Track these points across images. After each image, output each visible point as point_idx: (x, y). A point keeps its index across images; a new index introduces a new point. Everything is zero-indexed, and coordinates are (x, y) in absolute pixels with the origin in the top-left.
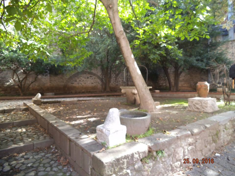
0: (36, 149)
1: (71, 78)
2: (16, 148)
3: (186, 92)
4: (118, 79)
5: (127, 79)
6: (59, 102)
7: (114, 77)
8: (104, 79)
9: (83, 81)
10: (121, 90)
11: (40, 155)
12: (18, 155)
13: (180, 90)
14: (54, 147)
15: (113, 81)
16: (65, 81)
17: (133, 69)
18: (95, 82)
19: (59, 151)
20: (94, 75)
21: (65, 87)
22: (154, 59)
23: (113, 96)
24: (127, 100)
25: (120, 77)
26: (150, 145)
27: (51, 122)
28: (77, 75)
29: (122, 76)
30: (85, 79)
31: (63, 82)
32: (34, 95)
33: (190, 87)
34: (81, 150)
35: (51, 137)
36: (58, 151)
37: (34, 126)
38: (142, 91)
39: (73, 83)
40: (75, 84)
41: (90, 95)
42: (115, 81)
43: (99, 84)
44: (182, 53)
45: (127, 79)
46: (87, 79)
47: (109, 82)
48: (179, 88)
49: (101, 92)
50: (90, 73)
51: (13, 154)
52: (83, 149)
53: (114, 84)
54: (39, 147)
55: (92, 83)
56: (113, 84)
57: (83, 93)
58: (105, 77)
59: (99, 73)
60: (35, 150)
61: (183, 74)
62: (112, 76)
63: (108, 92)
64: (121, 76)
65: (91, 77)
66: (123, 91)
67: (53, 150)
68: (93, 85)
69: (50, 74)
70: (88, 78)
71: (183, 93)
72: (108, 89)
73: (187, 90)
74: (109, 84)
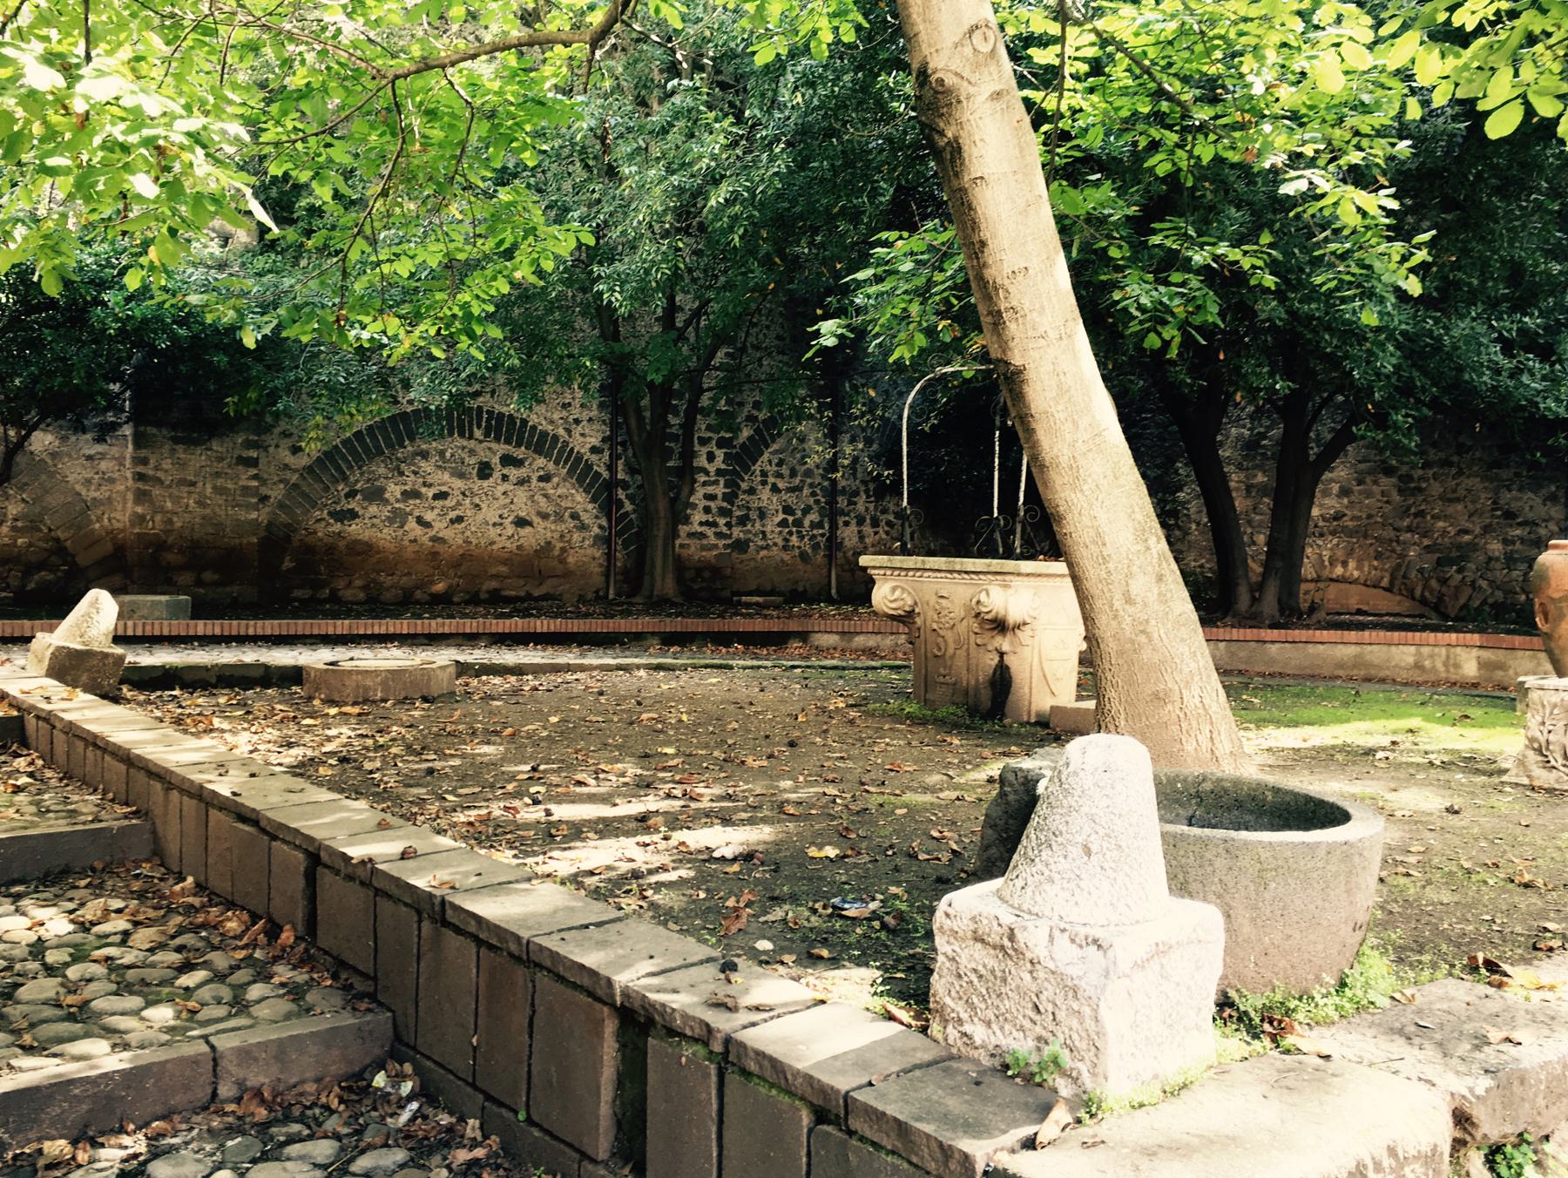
0: (238, 1100)
1: (332, 463)
2: (60, 1088)
3: (1361, 627)
4: (752, 491)
5: (832, 502)
6: (293, 676)
7: (719, 472)
8: (625, 485)
9: (442, 496)
10: (871, 582)
11: (301, 1158)
12: (82, 1157)
13: (1313, 609)
14: (407, 1088)
15: (707, 510)
16: (277, 493)
17: (1062, 390)
18: (545, 516)
19: (473, 1123)
20: (542, 444)
21: (276, 540)
22: (1159, 316)
23: (723, 639)
24: (926, 683)
25: (771, 480)
26: (1460, 1086)
27: (356, 852)
28: (404, 428)
29: (785, 470)
30: (458, 484)
31: (264, 499)
32: (58, 605)
33: (1388, 590)
34: (806, 1118)
35: (360, 983)
36: (462, 1120)
37: (136, 886)
38: (1129, 601)
39: (353, 515)
40: (371, 526)
41: (517, 624)
42: (723, 512)
43: (583, 527)
44: (1421, 270)
45: (832, 502)
46: (477, 484)
47: (679, 515)
48: (1306, 593)
49: (602, 603)
50: (504, 428)
51: (40, 1140)
52: (832, 1111)
53: (713, 540)
54: (258, 1078)
55: (521, 522)
56: (710, 532)
57: (441, 604)
58: (631, 470)
59: (587, 438)
60: (230, 1107)
61: (1340, 472)
62: (702, 461)
63: (657, 606)
64: (780, 463)
65: (507, 460)
66: (884, 595)
67: (405, 1116)
68: (530, 538)
69: (137, 418)
70: (485, 471)
71: (1353, 635)
72: (666, 584)
73: (1360, 612)
74: (675, 534)
